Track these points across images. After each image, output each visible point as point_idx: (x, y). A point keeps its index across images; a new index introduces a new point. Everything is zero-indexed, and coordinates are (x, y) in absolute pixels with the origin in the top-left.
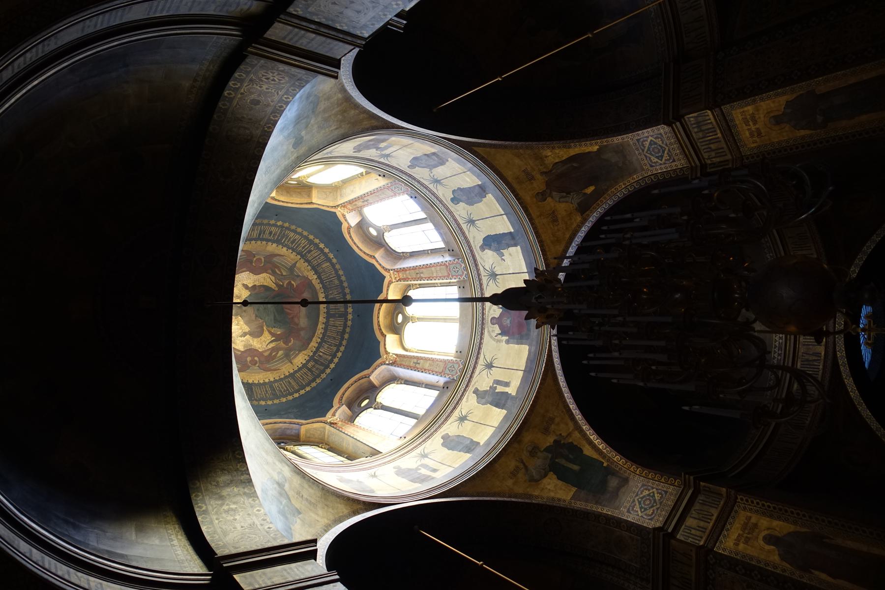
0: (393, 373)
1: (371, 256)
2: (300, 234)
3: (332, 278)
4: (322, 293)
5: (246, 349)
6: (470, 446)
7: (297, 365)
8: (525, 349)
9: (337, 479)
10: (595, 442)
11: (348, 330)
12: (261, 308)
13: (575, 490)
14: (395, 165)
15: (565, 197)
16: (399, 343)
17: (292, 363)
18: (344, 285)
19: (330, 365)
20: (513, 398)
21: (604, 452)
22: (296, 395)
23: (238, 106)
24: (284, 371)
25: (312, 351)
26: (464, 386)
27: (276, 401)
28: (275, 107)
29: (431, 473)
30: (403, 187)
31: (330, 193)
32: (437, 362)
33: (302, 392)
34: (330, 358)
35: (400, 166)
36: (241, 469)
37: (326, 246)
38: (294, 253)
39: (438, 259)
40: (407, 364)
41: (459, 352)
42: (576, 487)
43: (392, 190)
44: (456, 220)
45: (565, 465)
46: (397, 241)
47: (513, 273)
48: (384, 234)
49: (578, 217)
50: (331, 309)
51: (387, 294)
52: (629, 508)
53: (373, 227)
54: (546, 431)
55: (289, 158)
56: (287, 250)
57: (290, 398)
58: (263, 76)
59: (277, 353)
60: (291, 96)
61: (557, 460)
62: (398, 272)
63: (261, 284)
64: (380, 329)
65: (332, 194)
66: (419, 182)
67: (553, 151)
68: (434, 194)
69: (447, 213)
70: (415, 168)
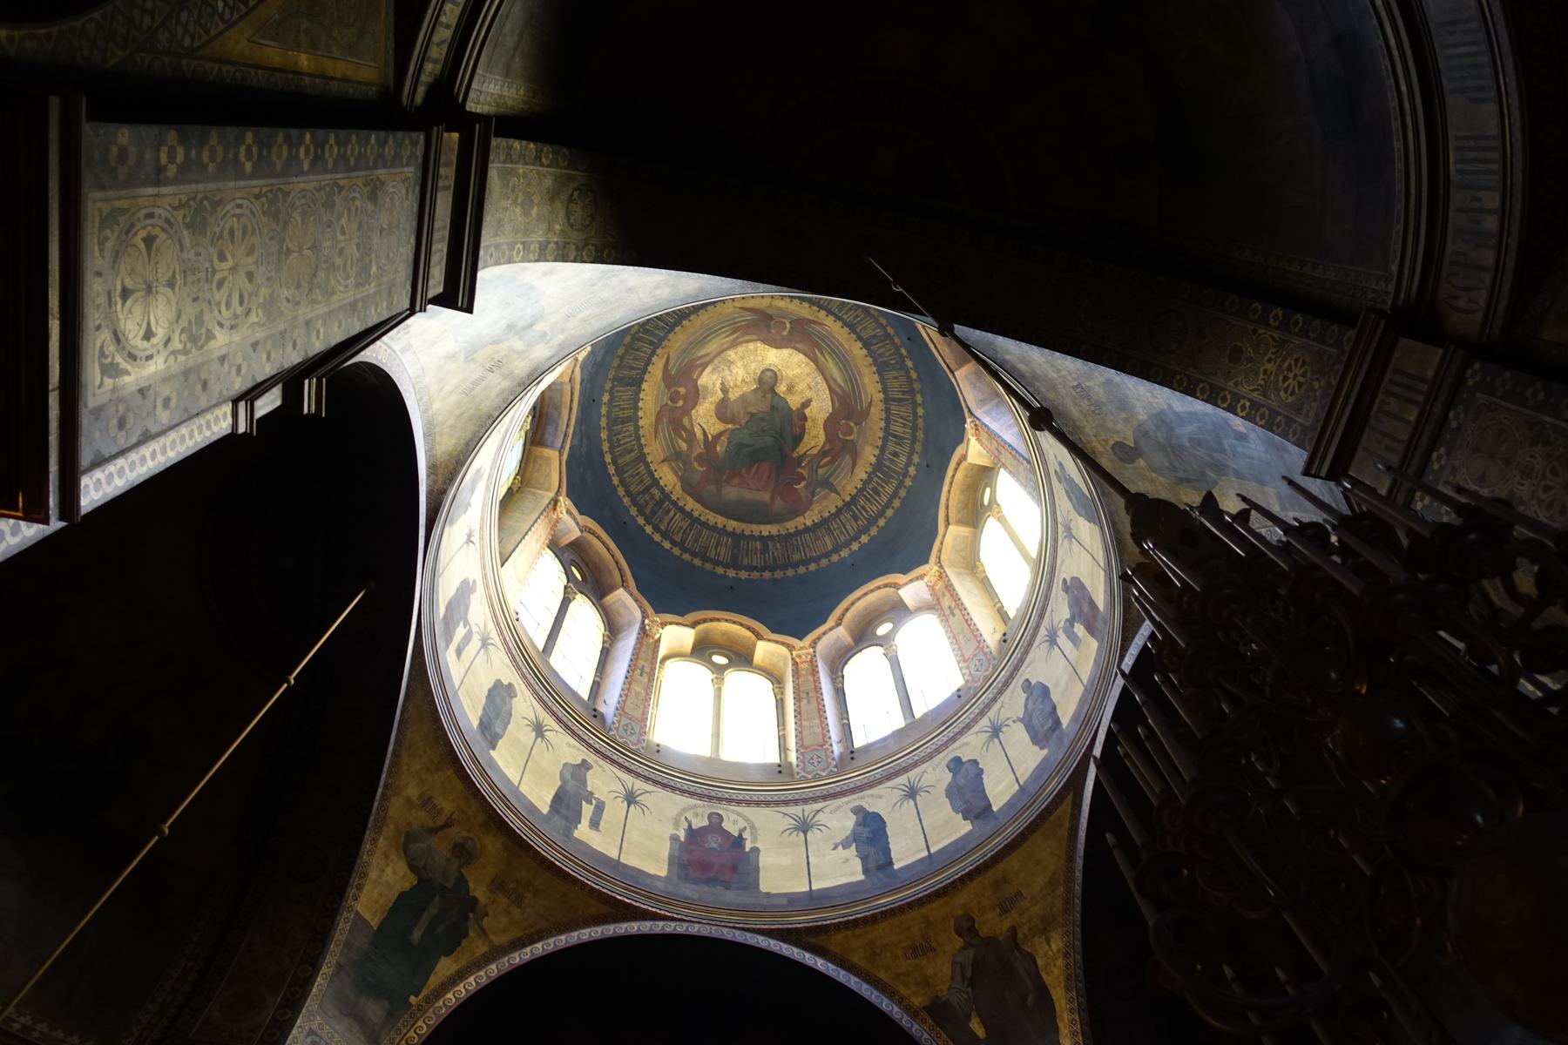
0: (625, 630)
1: (841, 620)
2: (889, 504)
3: (804, 551)
4: (779, 531)
5: (700, 388)
6: (491, 729)
7: (658, 471)
8: (657, 867)
9: (481, 467)
10: (462, 985)
11: (708, 566)
12: (764, 424)
13: (372, 924)
14: (1030, 657)
15: (963, 976)
16: (676, 650)
17: (663, 461)
18: (790, 570)
19: (651, 526)
20: (568, 832)
21: (437, 1000)
22: (608, 459)
23: (1228, 326)
24: (650, 445)
25: (678, 499)
26: (597, 746)
27: (604, 422)
28: (1224, 390)
29: (456, 645)
30: (981, 675)
31: (964, 558)
32: (642, 707)
33: (611, 469)
34: (663, 528)
35: (1029, 664)
36: (586, 249)
37: (863, 547)
38: (855, 491)
39: (834, 733)
40: (642, 654)
41: (658, 749)
42: (378, 928)
43: (975, 655)
44: (915, 765)
45: (425, 914)
46: (866, 670)
47: (808, 863)
48: (879, 647)
49: (920, 999)
50: (748, 543)
51: (769, 640)
52: (318, 1036)
53: (894, 628)
54: (498, 885)
55: (1095, 436)
56: (861, 480)
57: (605, 447)
58: (1297, 360)
59: (683, 439)
60: (1247, 414)
61: (437, 897)
62: (811, 661)
63: (807, 431)
64: (705, 621)
65: (962, 560)
66: (994, 700)
67: (1061, 955)
68: (968, 727)
69: (928, 751)
70: (1025, 692)
